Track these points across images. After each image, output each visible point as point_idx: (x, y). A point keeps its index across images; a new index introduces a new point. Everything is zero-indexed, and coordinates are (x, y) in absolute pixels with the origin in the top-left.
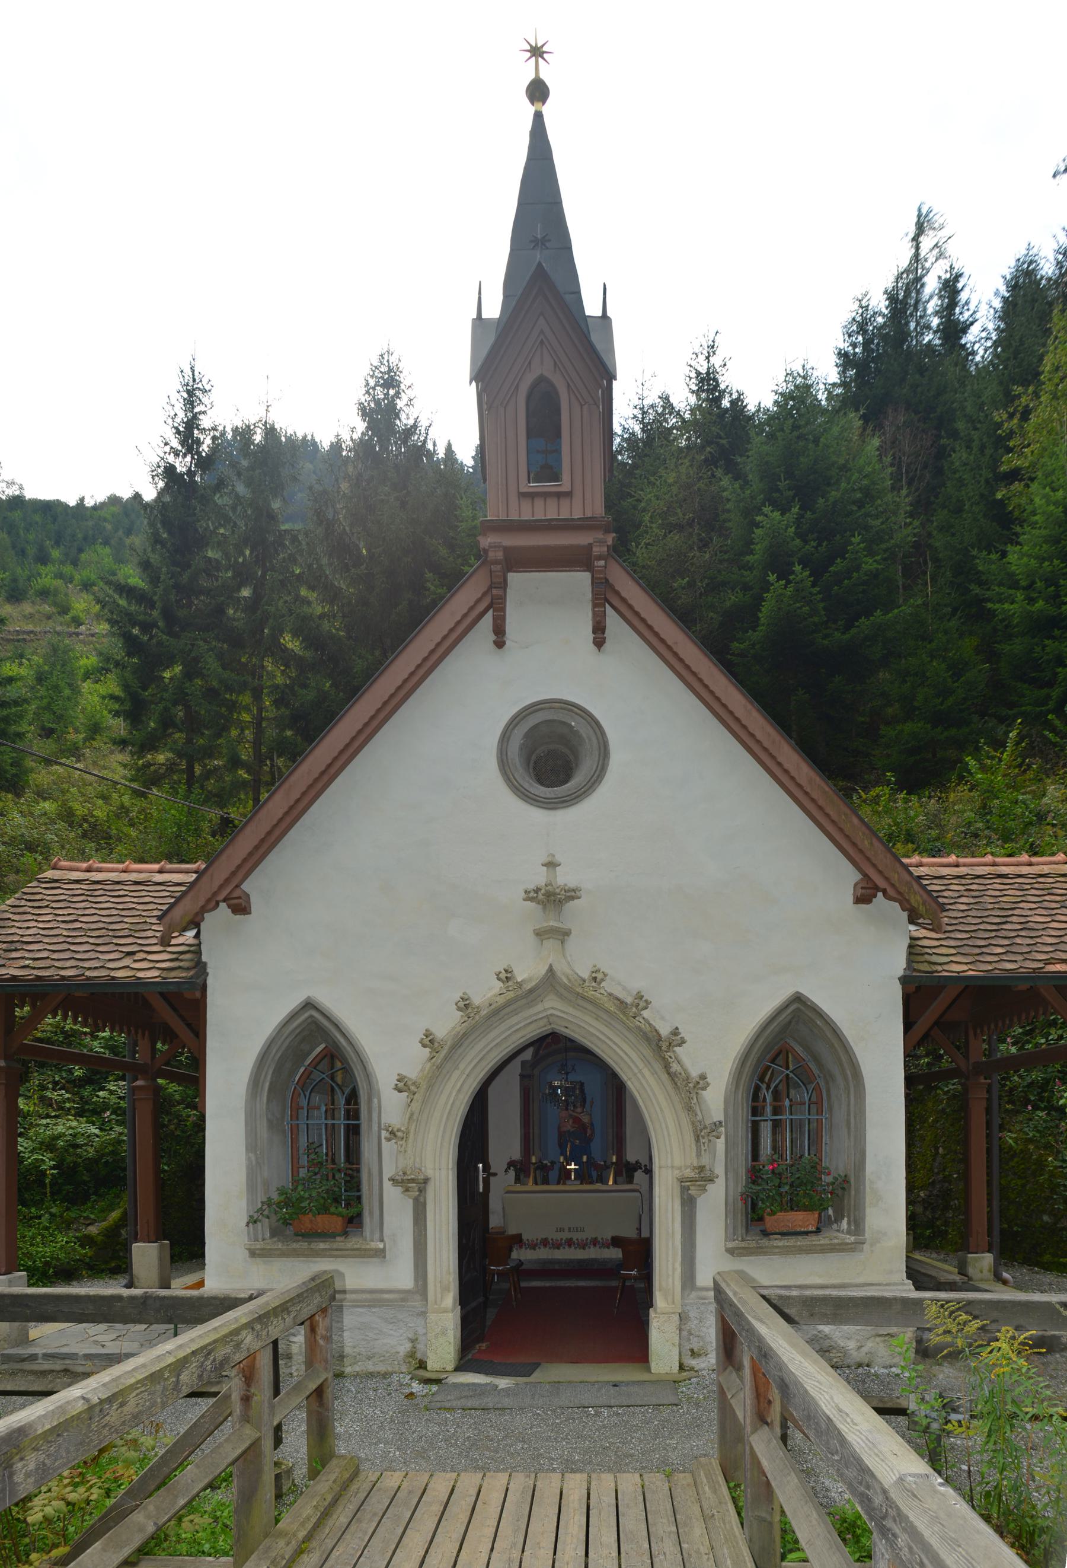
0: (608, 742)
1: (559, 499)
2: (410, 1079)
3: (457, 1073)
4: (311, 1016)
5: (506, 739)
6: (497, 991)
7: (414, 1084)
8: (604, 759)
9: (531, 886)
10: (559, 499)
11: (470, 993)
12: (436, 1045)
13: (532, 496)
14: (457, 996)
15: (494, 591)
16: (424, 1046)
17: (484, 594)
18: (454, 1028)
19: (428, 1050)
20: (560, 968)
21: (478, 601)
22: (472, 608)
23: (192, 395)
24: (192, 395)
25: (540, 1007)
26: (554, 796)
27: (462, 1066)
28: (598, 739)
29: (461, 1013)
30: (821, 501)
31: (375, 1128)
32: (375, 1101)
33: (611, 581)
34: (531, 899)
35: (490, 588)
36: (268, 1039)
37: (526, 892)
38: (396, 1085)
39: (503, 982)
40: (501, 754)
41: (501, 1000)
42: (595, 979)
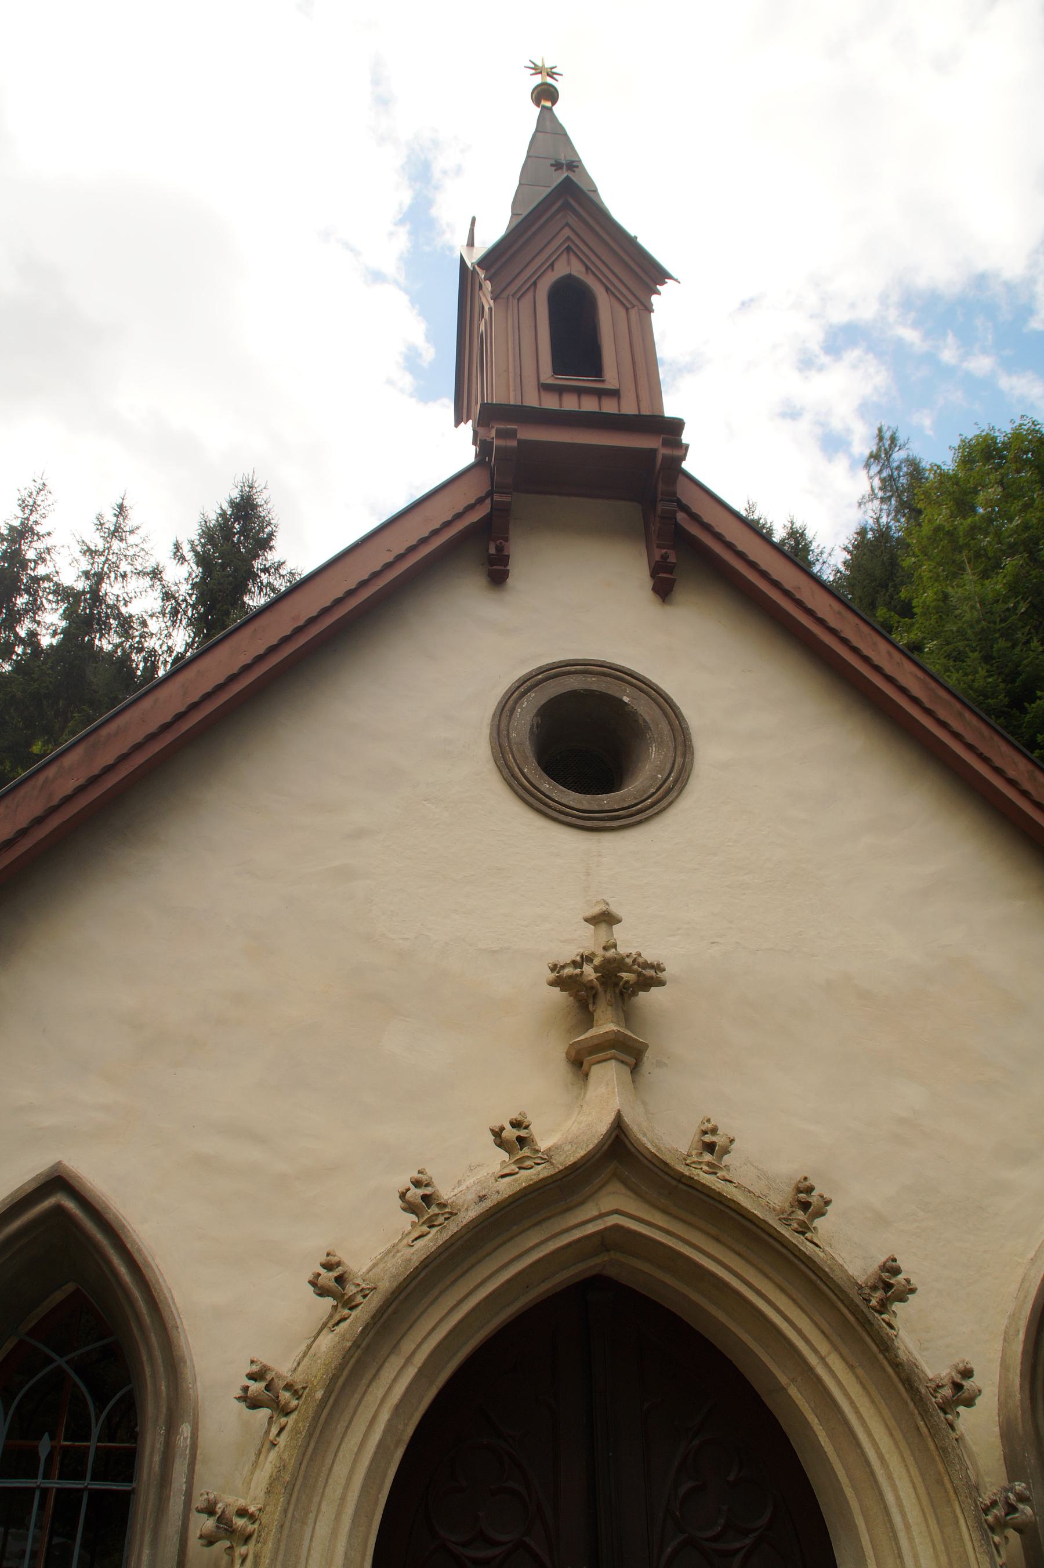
0: (688, 728)
1: (560, 395)
2: (279, 1376)
3: (395, 1363)
4: (59, 1209)
5: (506, 712)
6: (496, 1168)
7: (288, 1387)
8: (684, 756)
9: (569, 953)
10: (560, 395)
11: (432, 1172)
12: (351, 1290)
13: (560, 390)
14: (403, 1181)
15: (497, 497)
16: (322, 1292)
17: (480, 501)
18: (393, 1250)
19: (329, 1302)
20: (634, 1122)
21: (470, 508)
22: (458, 516)
23: (676, 280)
24: (676, 280)
25: (589, 1211)
26: (596, 808)
27: (407, 1346)
28: (670, 724)
29: (414, 1218)
30: (139, 671)
31: (176, 1505)
32: (186, 1429)
33: (684, 501)
34: (556, 983)
35: (490, 494)
36: (77, 1177)
37: (554, 968)
38: (246, 1389)
39: (509, 1151)
40: (498, 734)
41: (506, 1188)
42: (710, 1147)
